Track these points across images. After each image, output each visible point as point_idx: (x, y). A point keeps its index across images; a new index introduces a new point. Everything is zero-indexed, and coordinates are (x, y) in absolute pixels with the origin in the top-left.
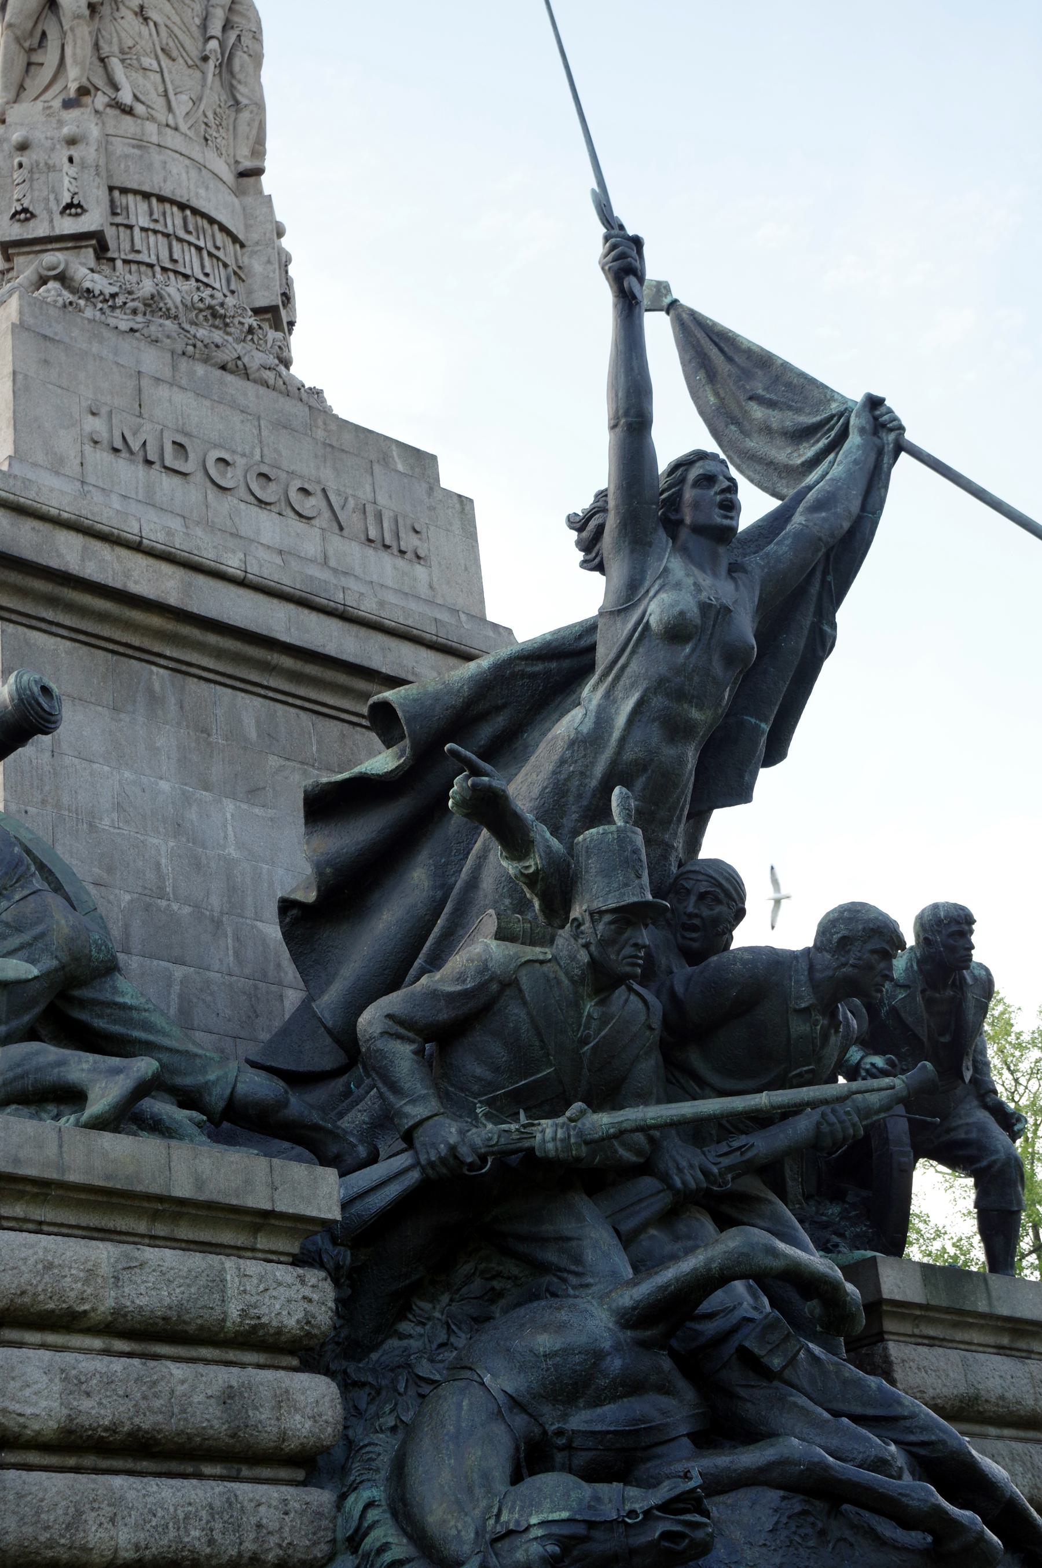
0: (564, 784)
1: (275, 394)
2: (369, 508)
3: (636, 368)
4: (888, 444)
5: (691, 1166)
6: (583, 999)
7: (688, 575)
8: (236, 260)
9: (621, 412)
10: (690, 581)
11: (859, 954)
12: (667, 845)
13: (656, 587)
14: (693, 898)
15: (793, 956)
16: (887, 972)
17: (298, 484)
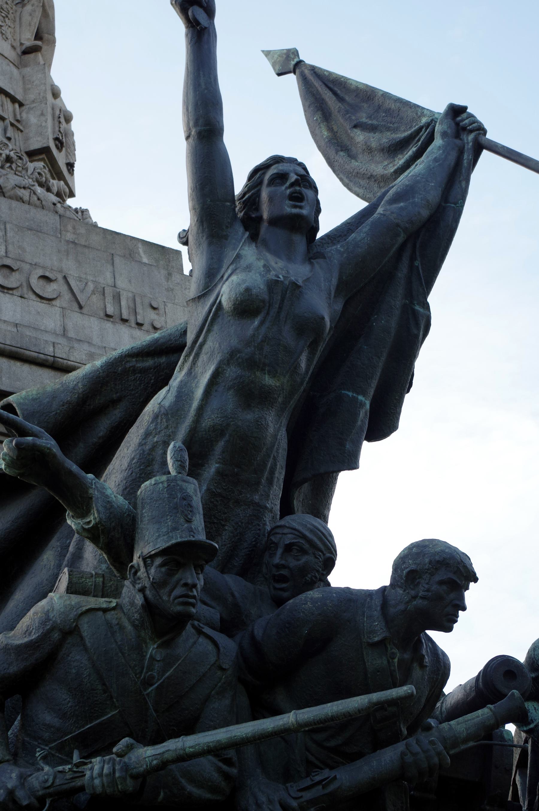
0: (149, 454)
1: (26, 206)
2: (108, 291)
3: (203, 84)
4: (468, 143)
5: (270, 801)
6: (146, 643)
7: (258, 259)
8: (15, 115)
9: (191, 124)
10: (261, 263)
11: (426, 586)
12: (258, 505)
13: (229, 271)
14: (280, 551)
15: (368, 594)
16: (458, 603)
17: (40, 272)
